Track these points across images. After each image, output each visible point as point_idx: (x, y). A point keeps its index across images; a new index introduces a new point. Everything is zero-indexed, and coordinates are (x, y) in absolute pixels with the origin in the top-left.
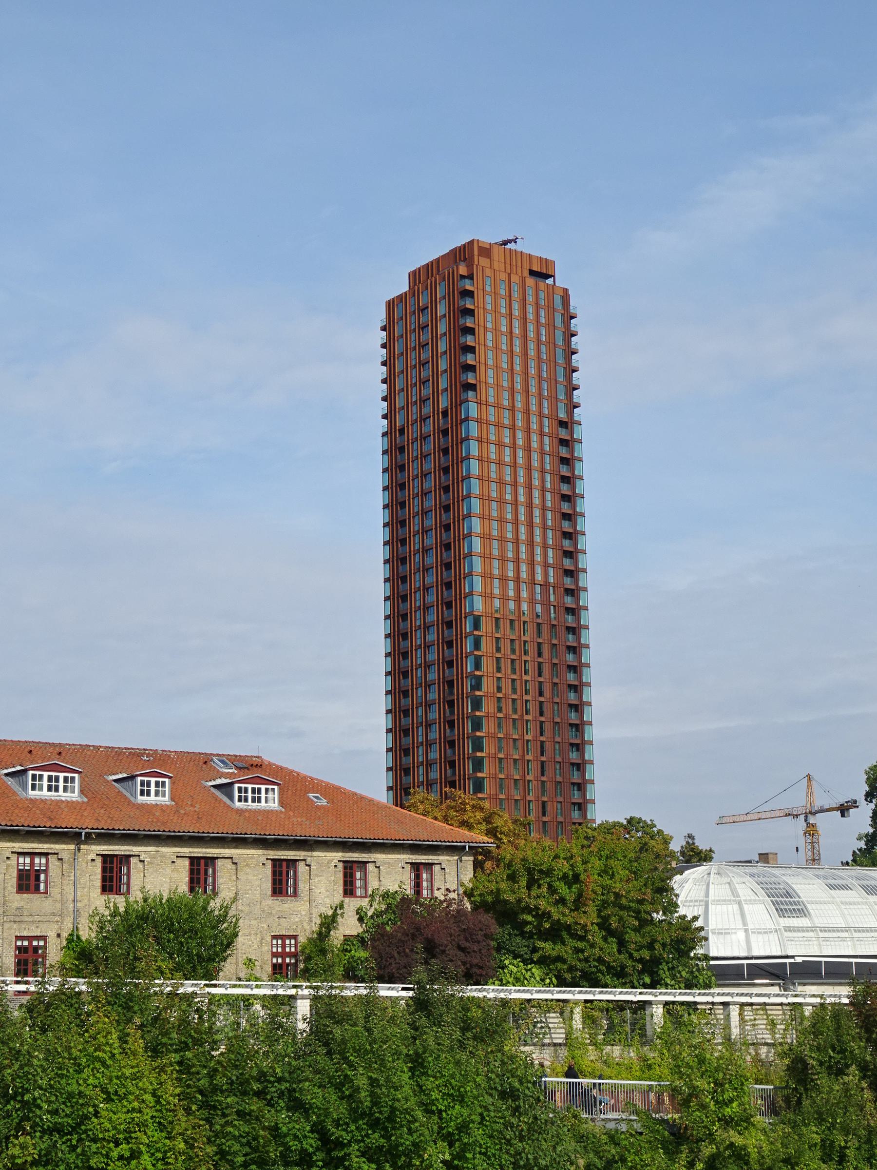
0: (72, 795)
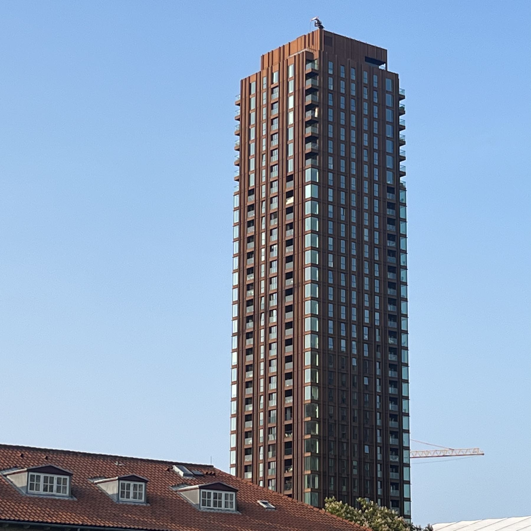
0: (64, 494)
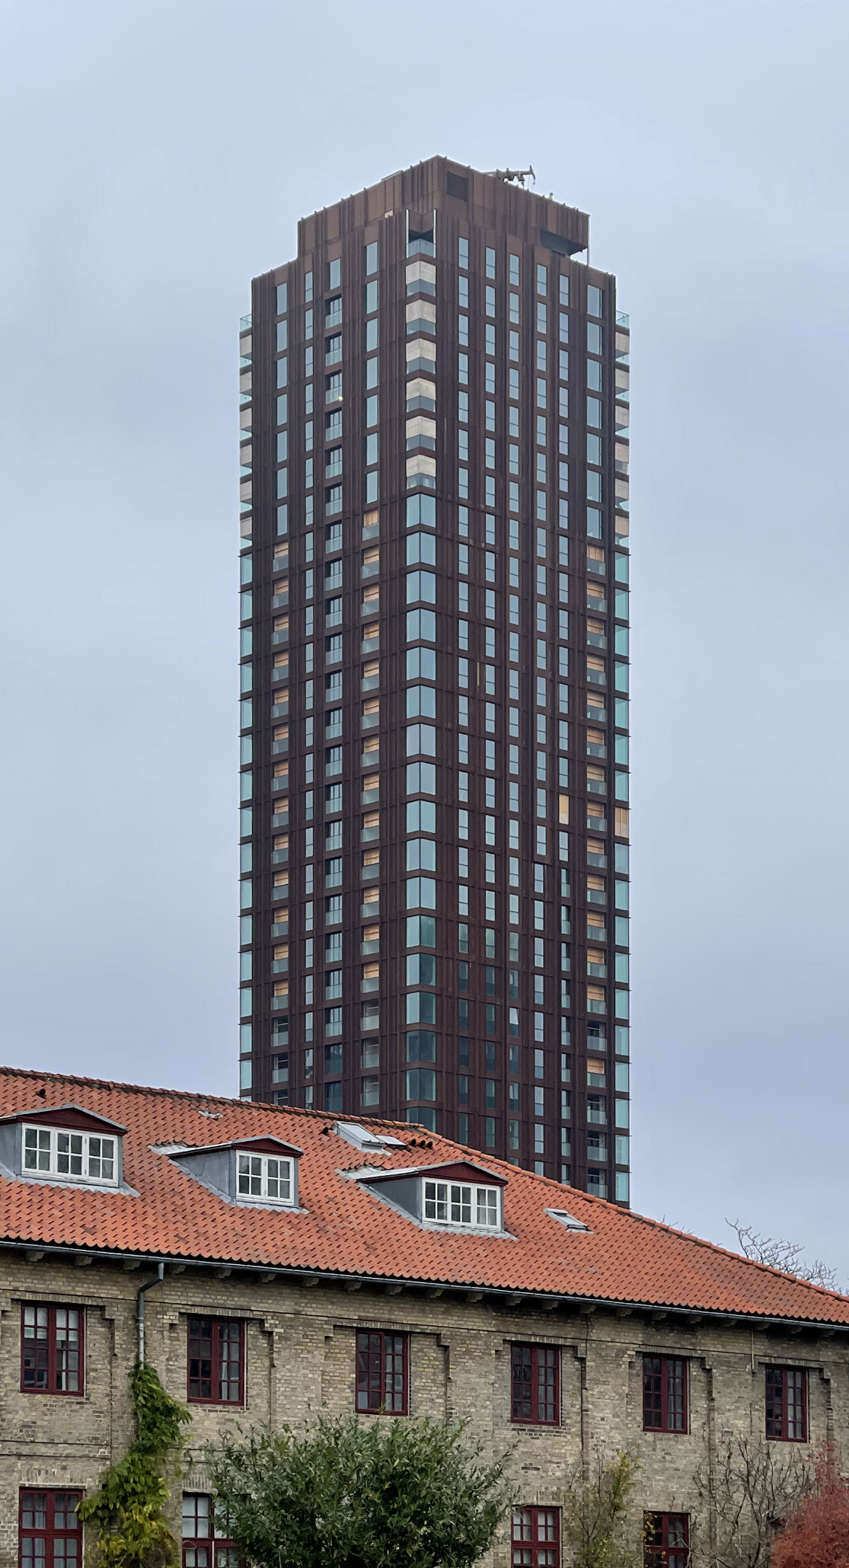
0: (107, 1181)
